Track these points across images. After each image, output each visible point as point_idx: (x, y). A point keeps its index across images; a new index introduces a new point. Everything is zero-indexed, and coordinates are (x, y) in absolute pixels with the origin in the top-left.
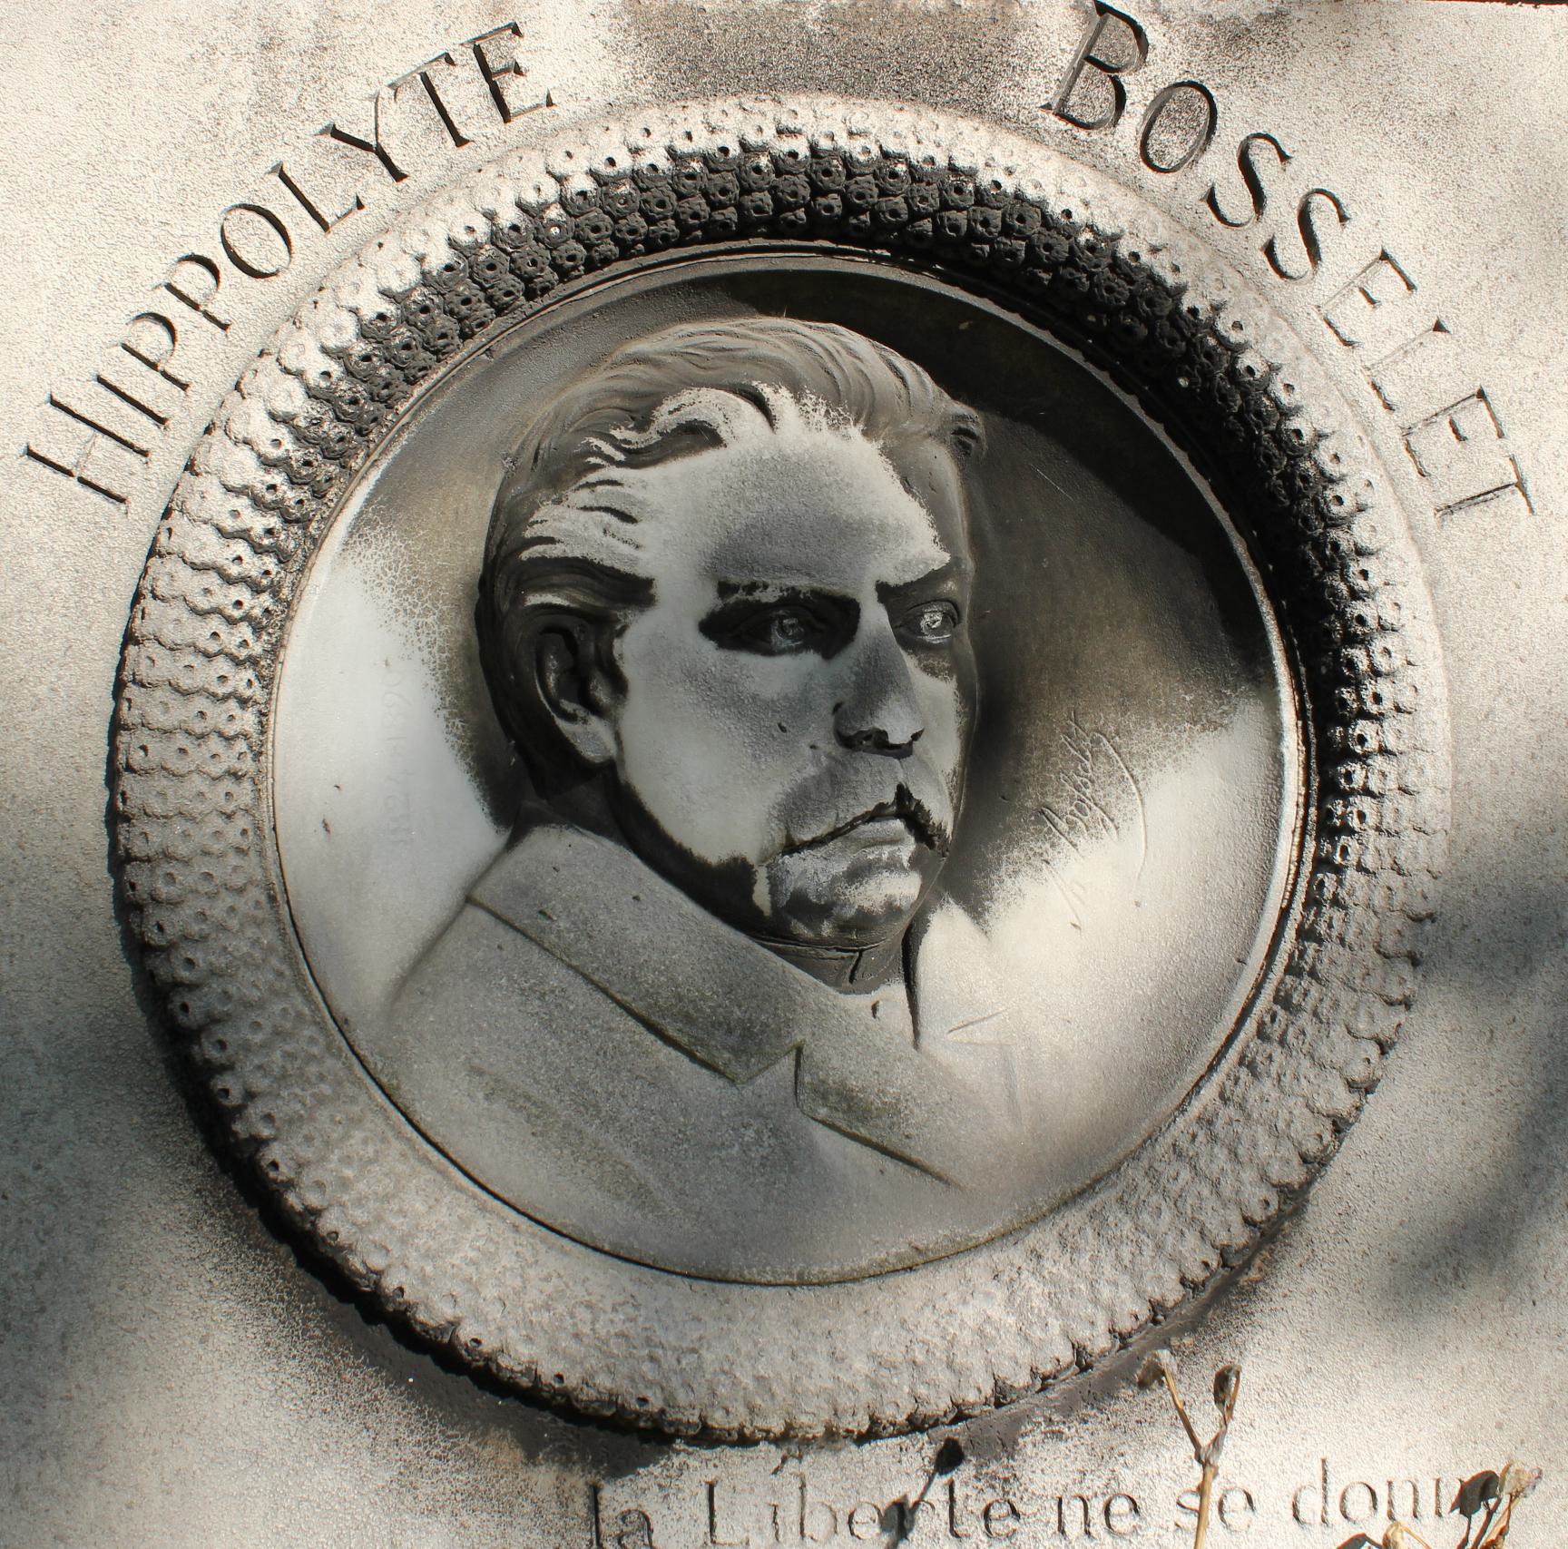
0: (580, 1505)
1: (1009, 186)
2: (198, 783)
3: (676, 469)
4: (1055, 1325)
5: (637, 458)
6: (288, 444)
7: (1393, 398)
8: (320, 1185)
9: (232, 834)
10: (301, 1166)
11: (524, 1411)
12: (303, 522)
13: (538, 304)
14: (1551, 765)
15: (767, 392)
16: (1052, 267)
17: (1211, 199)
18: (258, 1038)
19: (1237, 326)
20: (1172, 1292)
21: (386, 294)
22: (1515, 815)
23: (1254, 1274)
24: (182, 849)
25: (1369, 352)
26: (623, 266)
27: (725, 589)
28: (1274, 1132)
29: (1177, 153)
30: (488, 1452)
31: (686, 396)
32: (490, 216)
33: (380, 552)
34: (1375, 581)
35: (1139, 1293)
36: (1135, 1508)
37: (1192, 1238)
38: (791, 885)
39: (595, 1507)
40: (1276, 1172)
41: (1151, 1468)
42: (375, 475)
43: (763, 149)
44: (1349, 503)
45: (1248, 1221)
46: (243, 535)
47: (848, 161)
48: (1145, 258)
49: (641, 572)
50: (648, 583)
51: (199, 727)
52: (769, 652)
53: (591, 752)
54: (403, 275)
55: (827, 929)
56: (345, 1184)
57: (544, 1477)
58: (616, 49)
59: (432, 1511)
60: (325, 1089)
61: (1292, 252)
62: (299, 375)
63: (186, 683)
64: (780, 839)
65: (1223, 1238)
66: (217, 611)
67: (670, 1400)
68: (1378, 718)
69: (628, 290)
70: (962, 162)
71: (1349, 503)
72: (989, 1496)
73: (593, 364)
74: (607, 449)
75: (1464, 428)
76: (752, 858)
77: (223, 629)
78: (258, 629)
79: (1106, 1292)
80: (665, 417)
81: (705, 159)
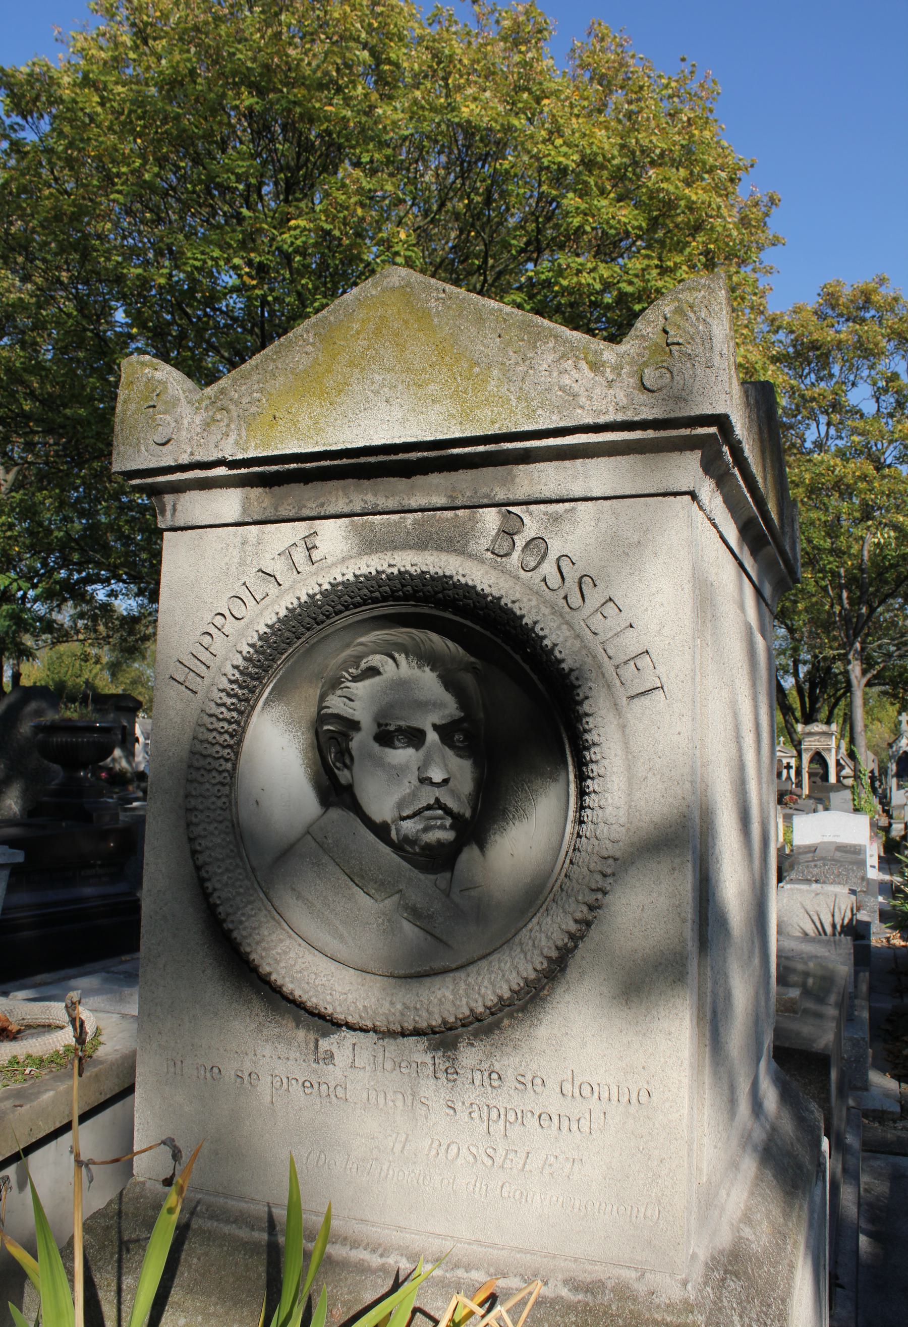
0: (312, 1045)
1: (463, 581)
2: (207, 786)
3: (367, 683)
4: (464, 1000)
5: (356, 679)
6: (238, 675)
7: (611, 654)
8: (232, 922)
9: (219, 803)
10: (228, 914)
11: (296, 1009)
12: (247, 700)
13: (321, 627)
14: (671, 800)
15: (396, 655)
16: (482, 609)
17: (544, 580)
18: (220, 871)
19: (542, 629)
20: (507, 995)
21: (267, 625)
22: (654, 819)
23: (545, 992)
24: (201, 807)
25: (602, 637)
26: (347, 613)
27: (379, 725)
28: (548, 937)
29: (533, 564)
30: (284, 1022)
31: (370, 658)
32: (299, 598)
33: (278, 710)
34: (591, 726)
35: (494, 992)
36: (500, 1078)
37: (514, 974)
38: (403, 832)
39: (316, 1047)
40: (545, 951)
41: (506, 1063)
42: (272, 685)
43: (383, 572)
44: (582, 695)
45: (535, 970)
46: (224, 705)
47: (411, 575)
48: (510, 605)
49: (356, 718)
50: (358, 723)
51: (208, 767)
52: (395, 748)
53: (343, 781)
54: (272, 619)
55: (417, 849)
56: (241, 922)
57: (301, 1034)
58: (346, 538)
59: (267, 1041)
60: (241, 890)
61: (575, 600)
62: (241, 652)
63: (204, 752)
64: (397, 815)
65: (525, 975)
66: (215, 729)
67: (334, 1009)
68: (592, 779)
69: (351, 621)
70: (447, 573)
71: (582, 695)
72: (447, 1064)
73: (348, 645)
74: (347, 676)
75: (639, 665)
76: (389, 822)
77: (218, 736)
78: (232, 736)
79: (483, 990)
80: (363, 665)
81: (365, 576)
